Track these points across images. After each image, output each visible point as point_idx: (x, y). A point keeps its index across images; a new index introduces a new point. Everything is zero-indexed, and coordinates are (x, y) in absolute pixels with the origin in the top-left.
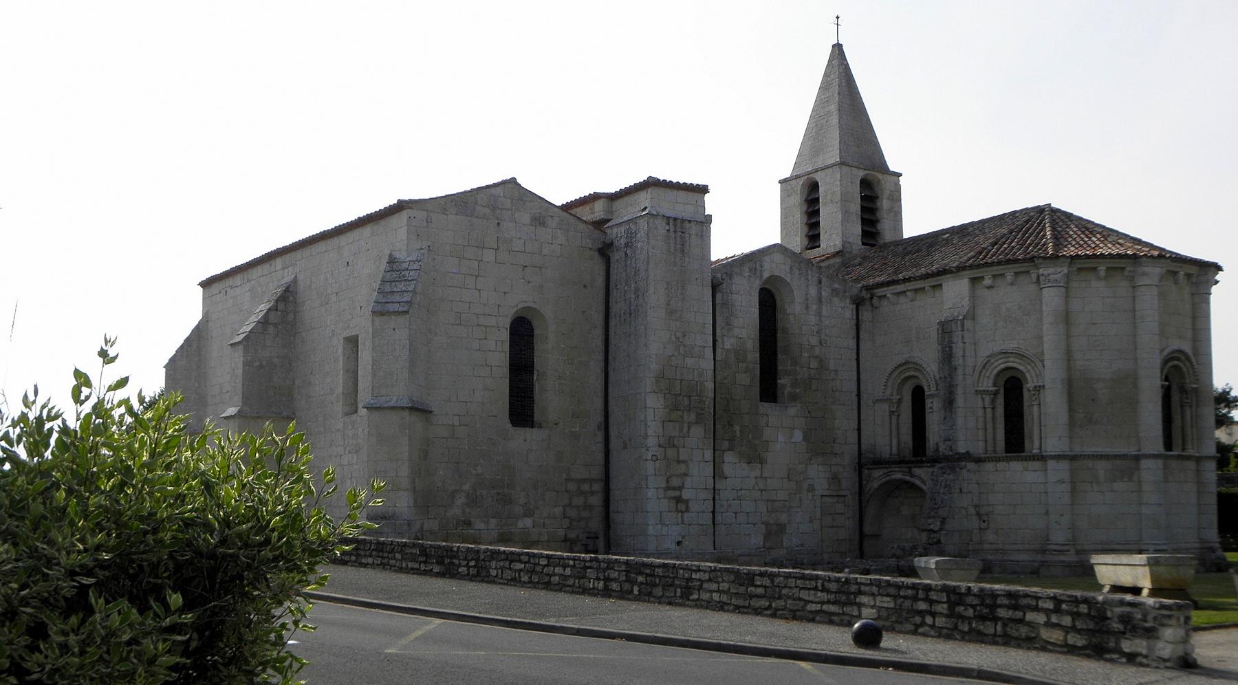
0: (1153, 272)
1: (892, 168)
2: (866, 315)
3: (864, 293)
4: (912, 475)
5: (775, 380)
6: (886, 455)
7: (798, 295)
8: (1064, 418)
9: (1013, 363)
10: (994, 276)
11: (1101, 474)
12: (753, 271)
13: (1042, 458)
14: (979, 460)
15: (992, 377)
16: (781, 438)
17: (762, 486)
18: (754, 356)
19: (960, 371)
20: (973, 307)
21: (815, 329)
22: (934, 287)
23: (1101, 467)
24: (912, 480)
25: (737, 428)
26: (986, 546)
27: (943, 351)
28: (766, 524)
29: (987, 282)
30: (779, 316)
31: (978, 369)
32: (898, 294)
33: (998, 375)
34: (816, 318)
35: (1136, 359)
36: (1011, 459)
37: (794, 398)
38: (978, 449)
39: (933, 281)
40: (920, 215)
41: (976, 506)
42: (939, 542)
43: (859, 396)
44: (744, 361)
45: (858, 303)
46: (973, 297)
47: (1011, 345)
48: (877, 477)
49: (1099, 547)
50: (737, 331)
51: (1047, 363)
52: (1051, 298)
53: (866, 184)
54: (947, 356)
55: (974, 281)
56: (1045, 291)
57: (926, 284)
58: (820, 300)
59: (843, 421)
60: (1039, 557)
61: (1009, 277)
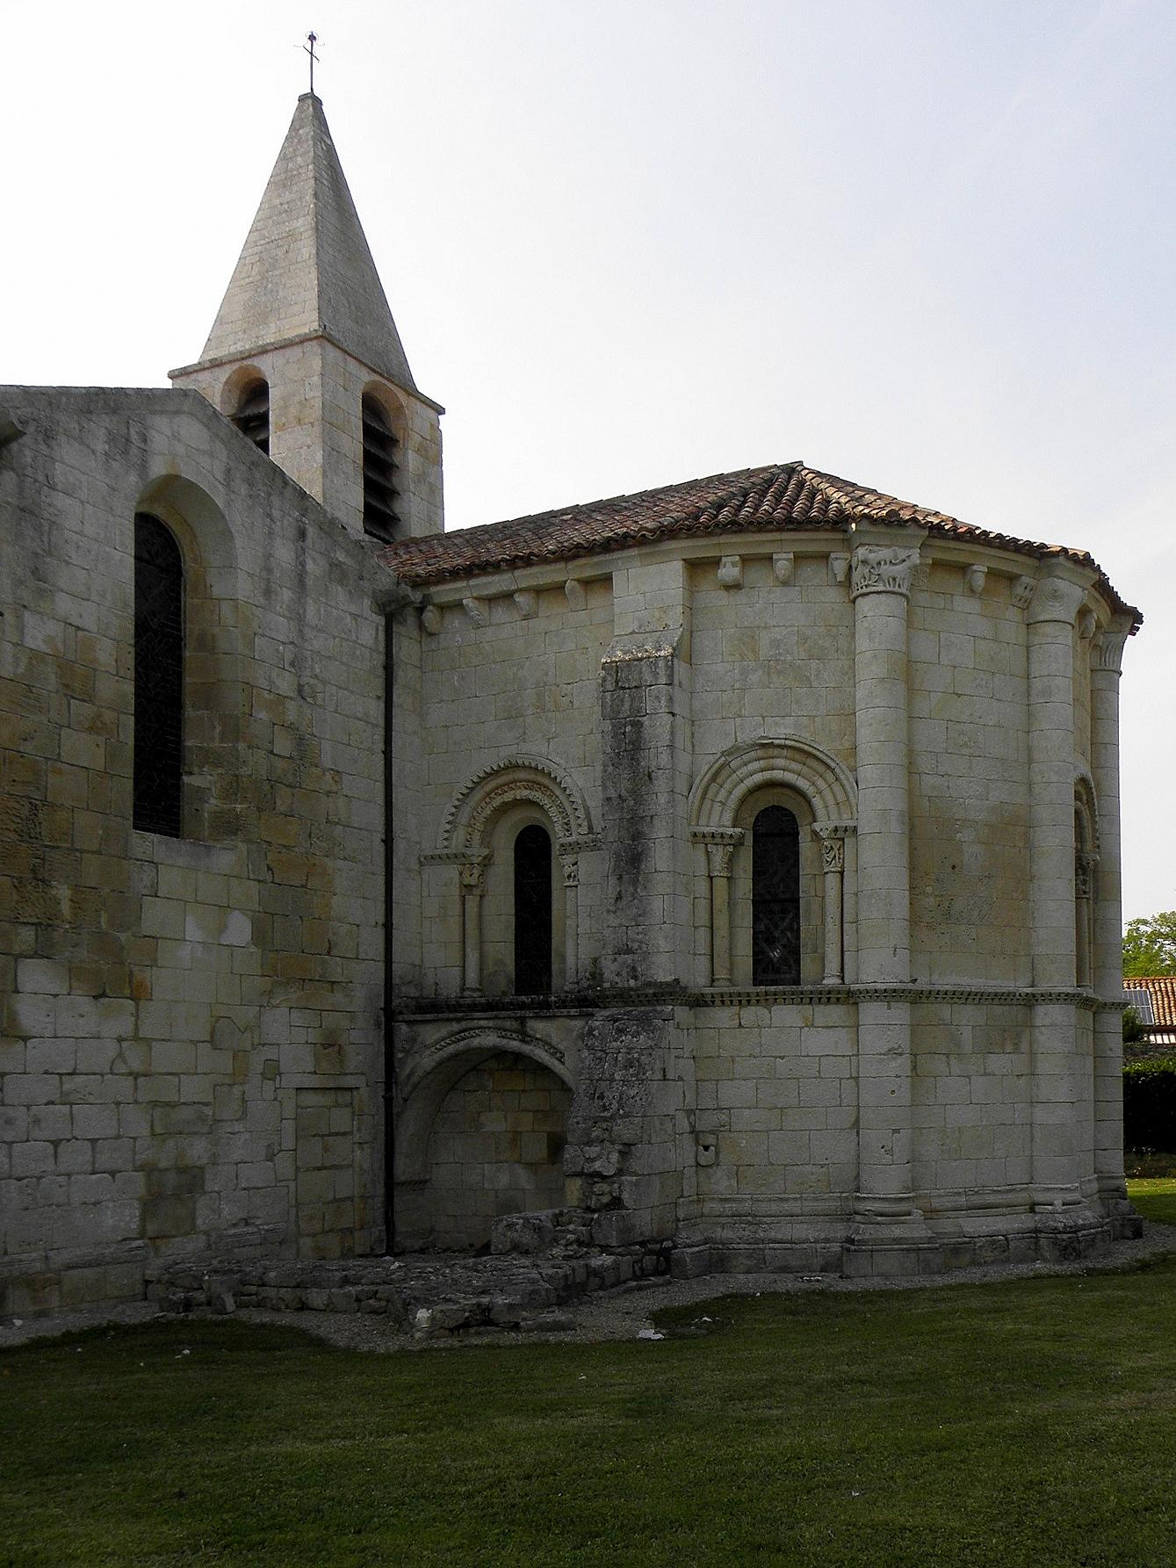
0: (1074, 593)
1: (424, 385)
2: (407, 648)
3: (406, 589)
4: (525, 1037)
6: (451, 990)
7: (246, 553)
8: (901, 908)
9: (787, 771)
10: (746, 560)
11: (967, 1034)
12: (121, 445)
13: (849, 997)
14: (699, 1002)
16: (193, 932)
17: (136, 1065)
19: (661, 784)
20: (691, 632)
22: (587, 583)
23: (967, 1019)
24: (526, 1049)
25: (63, 892)
27: (618, 733)
28: (148, 1169)
29: (729, 571)
30: (189, 601)
32: (491, 600)
33: (743, 801)
34: (281, 624)
35: (1030, 785)
36: (775, 999)
37: (229, 827)
38: (696, 978)
39: (588, 567)
40: (480, 487)
41: (690, 1112)
42: (616, 1203)
43: (388, 841)
44: (88, 698)
45: (392, 612)
46: (691, 610)
47: (781, 730)
48: (432, 1043)
49: (962, 1200)
50: (64, 605)
51: (864, 773)
52: (877, 618)
53: (373, 407)
54: (628, 744)
55: (697, 567)
58: (301, 582)
59: (350, 905)
60: (840, 1230)
61: (783, 565)
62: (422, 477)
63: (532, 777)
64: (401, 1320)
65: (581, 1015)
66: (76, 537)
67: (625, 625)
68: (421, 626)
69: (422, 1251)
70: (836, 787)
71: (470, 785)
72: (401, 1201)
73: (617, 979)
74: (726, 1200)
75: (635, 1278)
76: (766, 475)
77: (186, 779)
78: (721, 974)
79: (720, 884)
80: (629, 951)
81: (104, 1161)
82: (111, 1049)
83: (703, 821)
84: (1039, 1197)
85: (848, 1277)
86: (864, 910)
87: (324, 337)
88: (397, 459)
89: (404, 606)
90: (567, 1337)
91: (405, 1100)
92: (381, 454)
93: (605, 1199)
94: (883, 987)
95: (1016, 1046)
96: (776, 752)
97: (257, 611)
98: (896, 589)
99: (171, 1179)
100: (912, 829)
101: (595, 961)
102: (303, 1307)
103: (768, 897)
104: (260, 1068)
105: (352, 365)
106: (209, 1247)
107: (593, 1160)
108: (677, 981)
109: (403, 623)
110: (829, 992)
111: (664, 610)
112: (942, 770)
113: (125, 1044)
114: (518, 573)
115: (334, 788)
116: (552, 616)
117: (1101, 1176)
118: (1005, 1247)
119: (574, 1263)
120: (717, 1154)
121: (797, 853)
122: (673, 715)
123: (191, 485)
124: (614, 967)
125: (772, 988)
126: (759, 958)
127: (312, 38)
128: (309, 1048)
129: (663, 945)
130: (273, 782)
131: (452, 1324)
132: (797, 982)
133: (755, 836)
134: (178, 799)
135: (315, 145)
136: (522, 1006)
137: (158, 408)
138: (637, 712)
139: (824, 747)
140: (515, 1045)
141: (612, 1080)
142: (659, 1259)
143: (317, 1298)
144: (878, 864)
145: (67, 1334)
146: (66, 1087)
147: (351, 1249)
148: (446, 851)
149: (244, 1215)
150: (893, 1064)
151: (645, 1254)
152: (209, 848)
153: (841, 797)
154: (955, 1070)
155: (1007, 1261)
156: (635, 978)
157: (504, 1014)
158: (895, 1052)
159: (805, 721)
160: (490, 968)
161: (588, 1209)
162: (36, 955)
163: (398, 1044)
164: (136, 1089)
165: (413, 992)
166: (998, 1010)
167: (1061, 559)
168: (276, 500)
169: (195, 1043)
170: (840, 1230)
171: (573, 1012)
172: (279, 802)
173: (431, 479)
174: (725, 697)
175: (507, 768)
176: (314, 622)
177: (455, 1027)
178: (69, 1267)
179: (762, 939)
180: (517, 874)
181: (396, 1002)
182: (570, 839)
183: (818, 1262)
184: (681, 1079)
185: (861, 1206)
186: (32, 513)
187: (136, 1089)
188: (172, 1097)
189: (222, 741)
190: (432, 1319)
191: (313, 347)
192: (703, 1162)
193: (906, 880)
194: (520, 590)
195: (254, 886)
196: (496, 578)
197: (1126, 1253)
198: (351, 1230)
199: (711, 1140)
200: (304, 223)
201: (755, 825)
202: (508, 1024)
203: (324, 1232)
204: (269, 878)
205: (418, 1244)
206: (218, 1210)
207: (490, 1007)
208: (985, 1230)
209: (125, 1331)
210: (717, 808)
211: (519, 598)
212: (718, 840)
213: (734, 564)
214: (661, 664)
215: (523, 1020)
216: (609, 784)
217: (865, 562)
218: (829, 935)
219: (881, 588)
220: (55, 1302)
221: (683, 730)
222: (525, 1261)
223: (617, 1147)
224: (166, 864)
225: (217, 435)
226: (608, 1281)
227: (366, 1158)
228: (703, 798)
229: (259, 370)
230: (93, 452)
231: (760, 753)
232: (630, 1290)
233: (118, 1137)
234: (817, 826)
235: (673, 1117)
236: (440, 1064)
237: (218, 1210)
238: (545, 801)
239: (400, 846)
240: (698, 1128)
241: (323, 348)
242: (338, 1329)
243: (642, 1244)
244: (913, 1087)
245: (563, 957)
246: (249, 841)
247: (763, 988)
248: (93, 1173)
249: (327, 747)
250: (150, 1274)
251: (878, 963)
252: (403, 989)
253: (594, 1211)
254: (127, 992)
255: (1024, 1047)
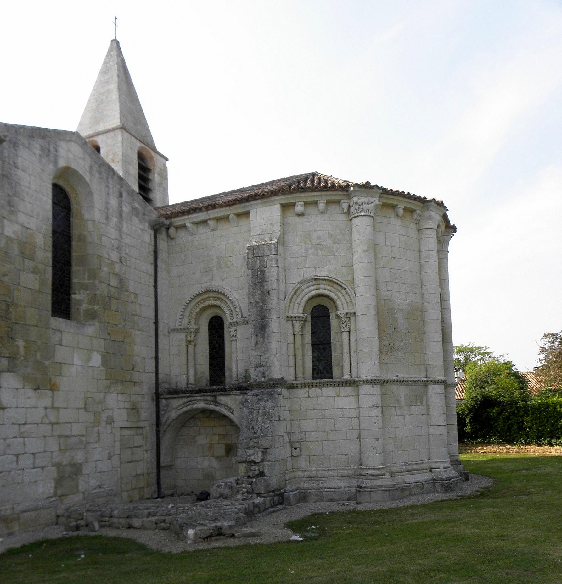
2: (163, 244)
4: (216, 403)
5: (69, 294)
6: (182, 384)
7: (98, 200)
9: (325, 290)
10: (306, 204)
11: (402, 397)
13: (355, 383)
14: (291, 387)
15: (303, 304)
16: (77, 361)
17: (52, 419)
18: (44, 254)
19: (273, 295)
20: (284, 234)
21: (116, 244)
22: (238, 215)
23: (403, 390)
24: (217, 408)
25: (21, 343)
26: (299, 474)
27: (254, 275)
28: (58, 465)
29: (299, 208)
30: (74, 221)
31: (289, 296)
32: (198, 224)
33: (307, 303)
34: (111, 231)
35: (422, 295)
36: (321, 386)
37: (92, 316)
38: (290, 377)
39: (239, 208)
40: (182, 186)
41: (289, 434)
43: (156, 323)
44: (32, 258)
46: (283, 224)
47: (323, 273)
48: (175, 408)
49: (404, 468)
50: (22, 218)
52: (362, 225)
53: (141, 157)
54: (259, 279)
55: (285, 207)
56: (355, 220)
57: (230, 211)
59: (142, 350)
61: (322, 205)
62: (160, 184)
63: (216, 295)
64: (178, 532)
65: (241, 394)
66: (27, 189)
67: (256, 231)
68: (168, 235)
69: (172, 495)
70: (346, 296)
71: (190, 299)
72: (163, 473)
73: (256, 378)
74: (305, 471)
75: (272, 507)
76: (306, 176)
77: (73, 296)
78: (300, 375)
79: (298, 337)
80: (261, 366)
81: (39, 462)
82: (42, 413)
83: (291, 311)
84: (433, 466)
85: (359, 503)
86: (359, 347)
87: (123, 128)
88: (151, 177)
89: (161, 226)
90: (257, 540)
91: (164, 431)
92: (145, 175)
93: (257, 472)
94: (370, 378)
95: (421, 402)
96: (321, 282)
97: (103, 225)
98: (369, 214)
99: (68, 469)
100: (378, 312)
101: (246, 371)
102: (130, 527)
103: (318, 343)
104: (105, 419)
105: (134, 140)
106: (84, 499)
107: (250, 456)
108: (282, 378)
109: (161, 234)
110: (346, 382)
111: (272, 225)
112: (389, 288)
113: (48, 410)
114: (209, 212)
115: (135, 301)
116: (224, 229)
117: (451, 455)
118: (422, 487)
119: (247, 501)
120: (301, 451)
121: (329, 324)
122: (278, 267)
123: (75, 172)
124: (255, 373)
125: (323, 380)
126: (315, 369)
127: (116, 18)
128: (126, 410)
129: (276, 363)
130: (110, 297)
131: (204, 536)
132: (331, 377)
133: (311, 317)
134: (69, 304)
135: (117, 58)
136: (214, 391)
137: (62, 138)
138: (262, 266)
139: (341, 279)
140: (212, 407)
141: (257, 421)
142: (280, 499)
143: (137, 523)
144: (366, 327)
145: (24, 546)
146: (22, 430)
147: (143, 496)
148: (180, 327)
149: (98, 484)
150: (375, 411)
151: (274, 496)
152: (83, 325)
153: (348, 300)
154: (399, 412)
155: (423, 493)
156: (264, 377)
157: (207, 394)
158: (375, 406)
159: (332, 269)
160: (199, 375)
161: (249, 477)
162: (9, 371)
163: (161, 407)
164: (53, 430)
165: (167, 386)
166: (414, 387)
167: (433, 203)
168: (110, 181)
169: (78, 409)
170: (354, 483)
171: (237, 392)
172: (112, 306)
173: (164, 185)
174: (298, 260)
175: (205, 292)
176: (126, 231)
177: (186, 400)
178: (24, 512)
179: (316, 360)
180: (209, 335)
181: (160, 390)
182: (234, 320)
183: (346, 497)
184: (285, 420)
185: (363, 472)
186: (8, 178)
187: (53, 430)
188: (69, 433)
189: (89, 279)
190: (196, 534)
191: (119, 132)
192: (294, 455)
193: (377, 333)
194: (210, 219)
195: (102, 340)
196: (200, 214)
197: (469, 489)
198: (143, 488)
199: (297, 445)
200: (113, 86)
201: (311, 313)
202: (209, 398)
203: (132, 489)
204: (108, 338)
205: (169, 492)
206: (88, 482)
207: (200, 391)
208: (414, 480)
209: (52, 543)
210: (296, 306)
211: (210, 222)
212: (297, 319)
213: (301, 205)
214: (272, 246)
215: (215, 396)
216: (251, 296)
217: (356, 203)
218: (344, 358)
219: (363, 214)
220: (16, 528)
221: (282, 274)
222: (226, 502)
223: (261, 450)
224: (65, 331)
225: (86, 152)
226: (262, 509)
227: (149, 457)
228: (291, 302)
229: (96, 142)
230: (35, 154)
231: (314, 282)
232: (271, 513)
233: (45, 452)
234: (338, 312)
235: (283, 436)
236: (179, 416)
237: (88, 482)
238: (222, 305)
239: (161, 325)
240: (292, 440)
241: (122, 132)
242: (152, 539)
243: (273, 491)
244: (383, 421)
245: (231, 370)
246: (100, 322)
247: (318, 381)
248: (34, 468)
249: (131, 283)
250: (59, 512)
251: (367, 369)
252: (163, 385)
253: (251, 478)
254: (49, 387)
255: (424, 403)
